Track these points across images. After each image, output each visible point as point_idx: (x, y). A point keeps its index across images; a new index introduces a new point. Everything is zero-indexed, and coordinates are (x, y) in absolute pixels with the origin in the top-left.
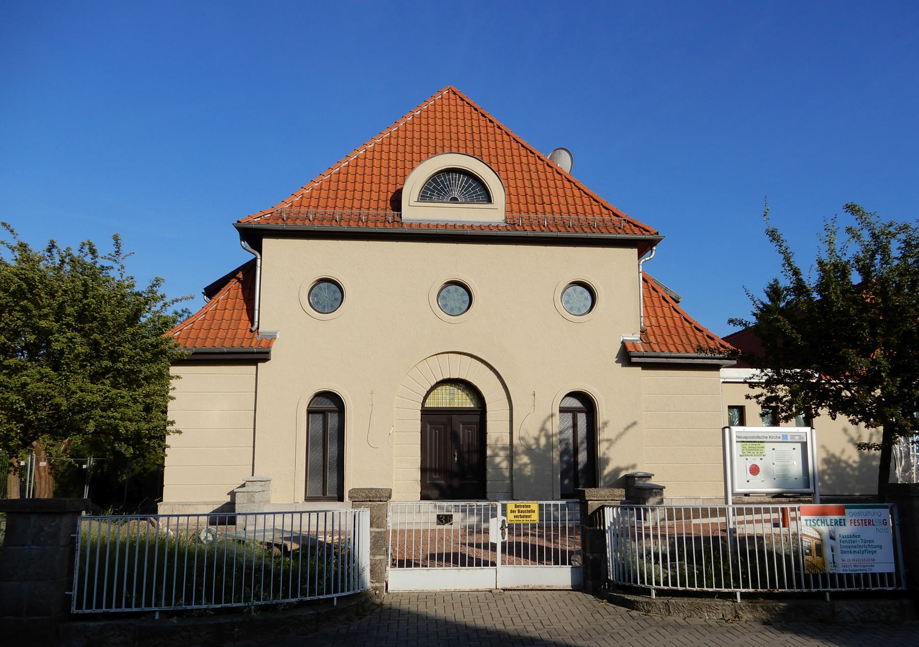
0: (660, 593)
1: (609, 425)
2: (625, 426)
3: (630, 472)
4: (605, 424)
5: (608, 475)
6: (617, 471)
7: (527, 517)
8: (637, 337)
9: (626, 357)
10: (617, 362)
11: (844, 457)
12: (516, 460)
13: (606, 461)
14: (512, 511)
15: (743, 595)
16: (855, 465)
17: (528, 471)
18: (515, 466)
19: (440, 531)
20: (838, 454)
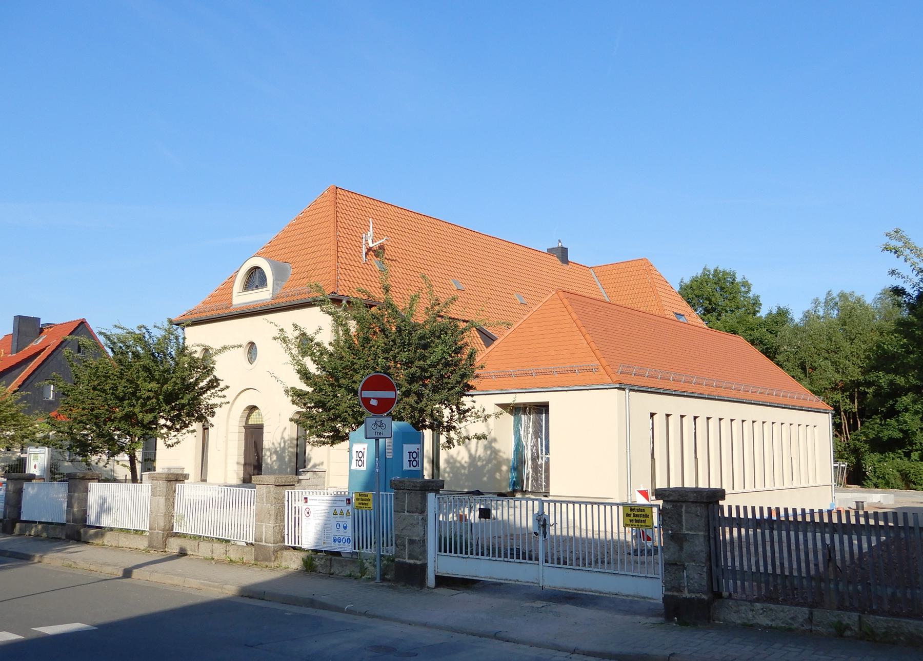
7: (641, 521)
11: (459, 459)
13: (310, 460)
16: (466, 465)
19: (482, 525)
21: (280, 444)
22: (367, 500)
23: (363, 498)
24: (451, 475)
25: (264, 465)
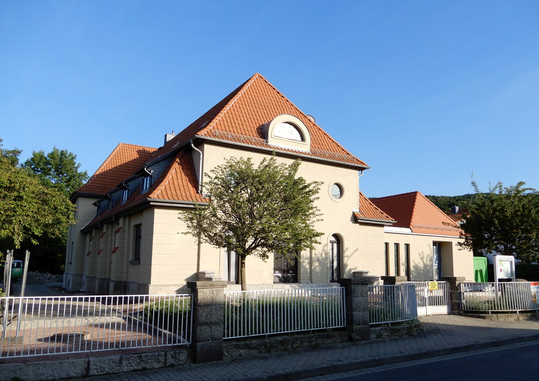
0: (492, 313)
1: (348, 249)
2: (354, 250)
3: (355, 271)
4: (347, 249)
5: (347, 272)
6: (351, 270)
8: (358, 210)
9: (355, 219)
10: (351, 221)
11: (419, 266)
12: (314, 264)
13: (347, 266)
14: (430, 285)
15: (520, 312)
17: (318, 269)
18: (313, 268)
20: (418, 264)
21: (321, 255)
22: (435, 285)
23: (433, 284)
24: (416, 273)
25: (302, 269)
